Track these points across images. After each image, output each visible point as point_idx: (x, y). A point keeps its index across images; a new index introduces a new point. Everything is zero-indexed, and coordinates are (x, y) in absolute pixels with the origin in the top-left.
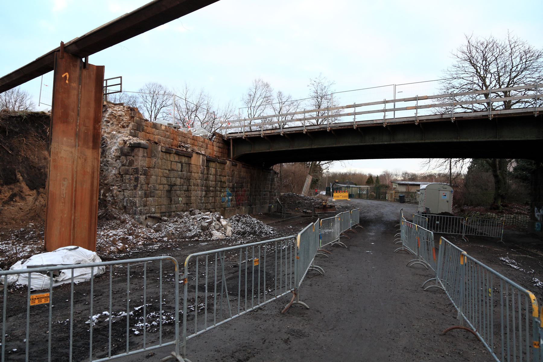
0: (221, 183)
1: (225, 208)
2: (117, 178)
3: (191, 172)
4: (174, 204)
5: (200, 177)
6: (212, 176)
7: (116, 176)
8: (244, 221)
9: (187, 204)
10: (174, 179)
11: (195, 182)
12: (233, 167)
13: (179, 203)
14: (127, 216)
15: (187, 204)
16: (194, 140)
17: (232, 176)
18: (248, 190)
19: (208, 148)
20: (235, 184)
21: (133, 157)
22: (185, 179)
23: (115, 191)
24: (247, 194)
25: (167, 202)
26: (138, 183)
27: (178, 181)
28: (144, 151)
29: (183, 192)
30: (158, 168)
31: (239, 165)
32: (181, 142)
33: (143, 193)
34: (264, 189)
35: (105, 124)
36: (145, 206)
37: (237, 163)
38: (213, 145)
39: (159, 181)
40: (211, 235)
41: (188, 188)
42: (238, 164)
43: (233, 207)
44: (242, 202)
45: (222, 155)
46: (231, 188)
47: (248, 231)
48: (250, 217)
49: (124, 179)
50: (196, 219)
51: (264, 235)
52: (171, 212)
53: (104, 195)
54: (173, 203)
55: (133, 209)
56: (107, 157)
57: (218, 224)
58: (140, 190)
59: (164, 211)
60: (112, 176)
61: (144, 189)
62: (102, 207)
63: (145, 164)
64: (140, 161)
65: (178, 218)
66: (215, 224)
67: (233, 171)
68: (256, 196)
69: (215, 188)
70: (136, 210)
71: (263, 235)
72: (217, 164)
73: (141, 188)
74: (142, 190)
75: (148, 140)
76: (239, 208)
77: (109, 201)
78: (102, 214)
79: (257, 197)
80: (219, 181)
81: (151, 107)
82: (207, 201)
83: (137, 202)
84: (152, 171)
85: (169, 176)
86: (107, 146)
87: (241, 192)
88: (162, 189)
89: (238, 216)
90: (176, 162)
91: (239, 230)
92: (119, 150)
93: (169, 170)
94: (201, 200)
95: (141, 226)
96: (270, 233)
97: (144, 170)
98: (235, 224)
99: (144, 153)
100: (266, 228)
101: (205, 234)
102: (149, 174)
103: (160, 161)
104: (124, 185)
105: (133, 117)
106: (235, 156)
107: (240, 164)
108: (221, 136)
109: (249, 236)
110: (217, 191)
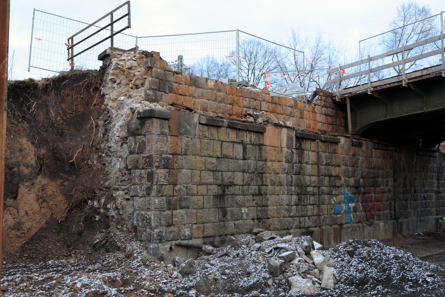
0: (330, 179)
1: (341, 225)
2: (123, 176)
3: (266, 161)
4: (232, 220)
5: (284, 169)
6: (309, 166)
7: (122, 173)
8: (365, 254)
9: (259, 219)
10: (228, 173)
11: (274, 178)
12: (354, 147)
13: (241, 218)
14: (135, 246)
15: (259, 219)
16: (276, 104)
17: (354, 165)
18: (389, 191)
19: (305, 117)
20: (361, 180)
21: (145, 135)
22: (254, 173)
23: (119, 200)
24: (388, 197)
25: (217, 217)
26: (152, 183)
27: (239, 178)
28: (162, 125)
29: (250, 197)
30: (194, 155)
31: (367, 145)
32: (247, 108)
33: (164, 202)
34: (424, 186)
35: (110, 85)
36: (169, 225)
37: (362, 141)
38: (314, 112)
39: (197, 179)
40: (289, 285)
41: (260, 190)
42: (364, 142)
43: (358, 222)
44: (379, 212)
45: (333, 128)
46: (351, 187)
47: (371, 277)
48: (379, 246)
49: (133, 177)
50: (264, 251)
51: (411, 287)
52: (226, 235)
53: (104, 206)
54: (229, 217)
55: (146, 231)
56: (110, 140)
57: (306, 261)
58: (157, 196)
59: (211, 234)
60: (115, 173)
61: (165, 193)
62: (102, 228)
63: (165, 149)
64: (154, 143)
65: (232, 247)
66: (299, 261)
67: (354, 155)
68: (406, 200)
69: (319, 187)
70: (150, 233)
71: (406, 287)
72: (320, 143)
73: (160, 191)
74: (162, 196)
75: (171, 105)
76: (371, 225)
77: (113, 217)
78: (101, 242)
79: (409, 202)
80: (325, 176)
81: (248, 76)
82: (303, 213)
83: (152, 218)
84: (181, 160)
85: (219, 169)
86: (111, 123)
87: (375, 193)
88: (205, 192)
89: (351, 244)
90: (232, 142)
91: (351, 275)
92: (126, 127)
93: (218, 158)
94: (289, 211)
95: (156, 264)
96: (425, 281)
97: (164, 158)
98: (342, 260)
99: (162, 127)
100: (416, 270)
101: (276, 283)
102: (176, 166)
103: (197, 141)
104: (132, 187)
105: (150, 68)
106: (358, 128)
107: (369, 143)
108: (330, 96)
109: (374, 288)
110: (323, 193)
